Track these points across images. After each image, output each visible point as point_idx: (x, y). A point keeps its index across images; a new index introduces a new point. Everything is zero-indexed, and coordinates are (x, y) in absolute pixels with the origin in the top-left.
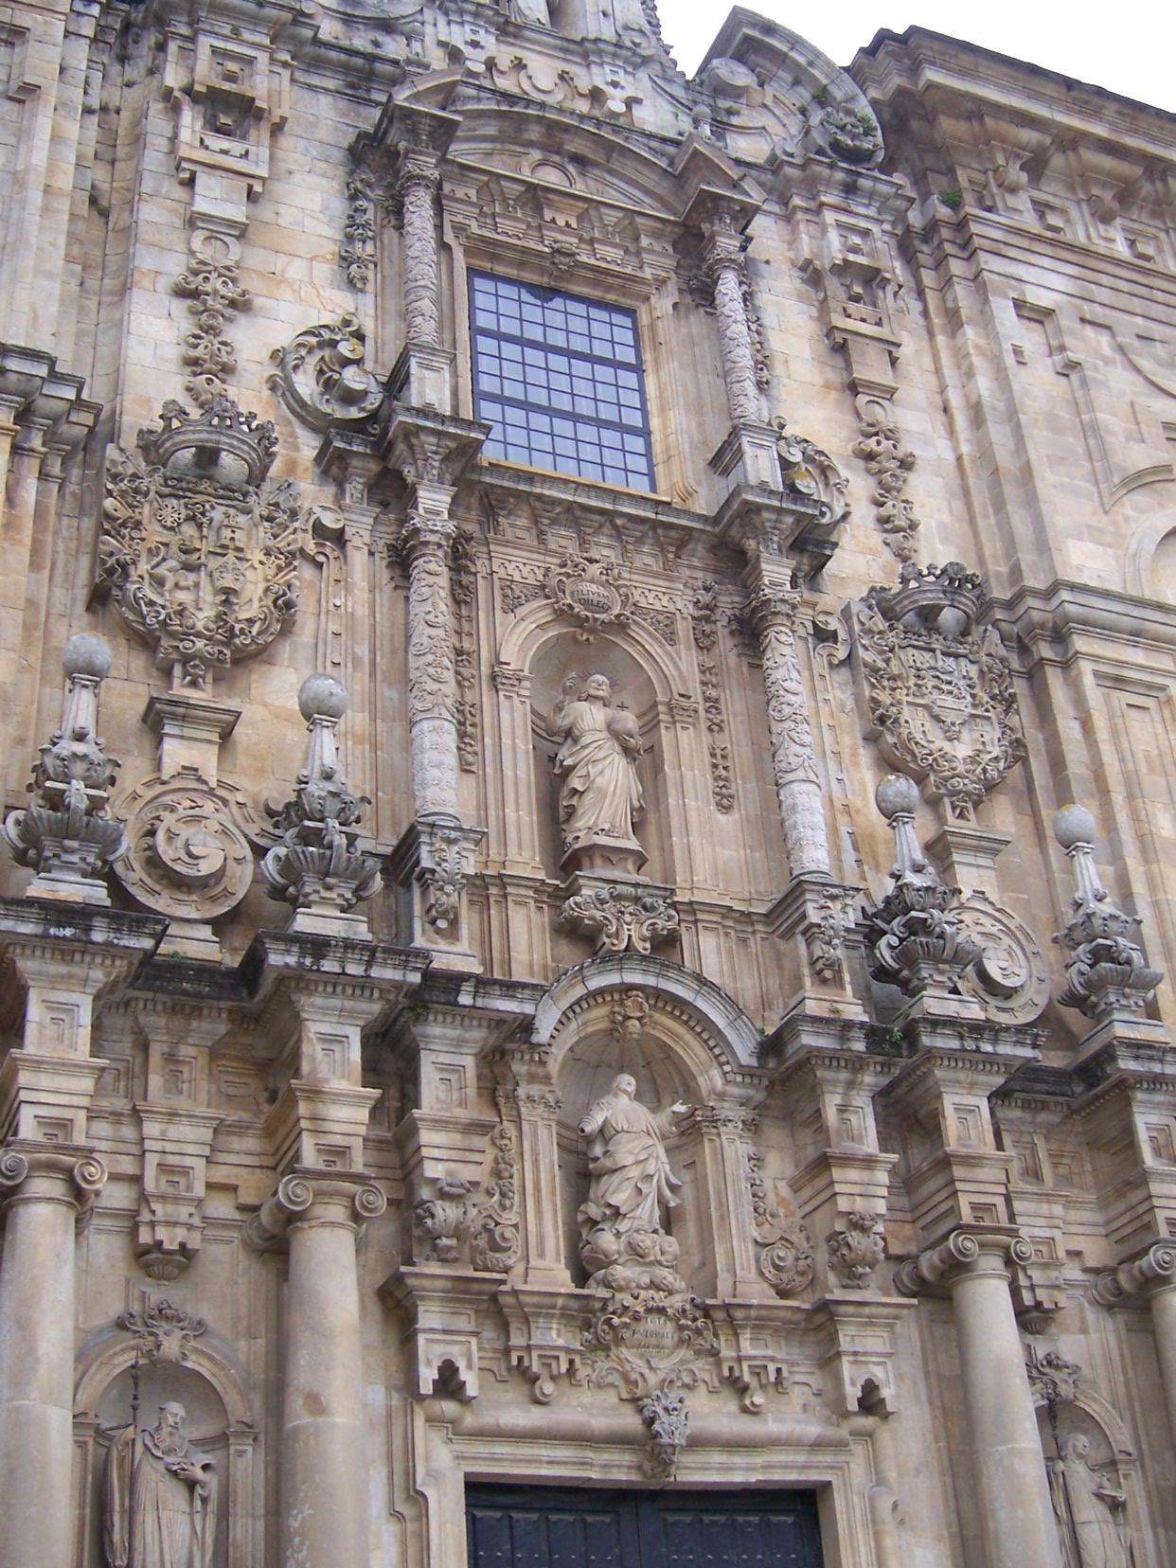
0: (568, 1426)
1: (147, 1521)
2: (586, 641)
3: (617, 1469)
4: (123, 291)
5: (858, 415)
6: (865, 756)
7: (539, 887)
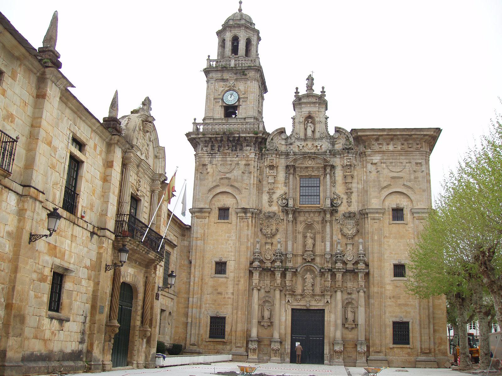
0: (301, 304)
1: (265, 313)
2: (309, 226)
3: (305, 308)
4: (262, 193)
5: (346, 187)
6: (340, 233)
7: (301, 255)
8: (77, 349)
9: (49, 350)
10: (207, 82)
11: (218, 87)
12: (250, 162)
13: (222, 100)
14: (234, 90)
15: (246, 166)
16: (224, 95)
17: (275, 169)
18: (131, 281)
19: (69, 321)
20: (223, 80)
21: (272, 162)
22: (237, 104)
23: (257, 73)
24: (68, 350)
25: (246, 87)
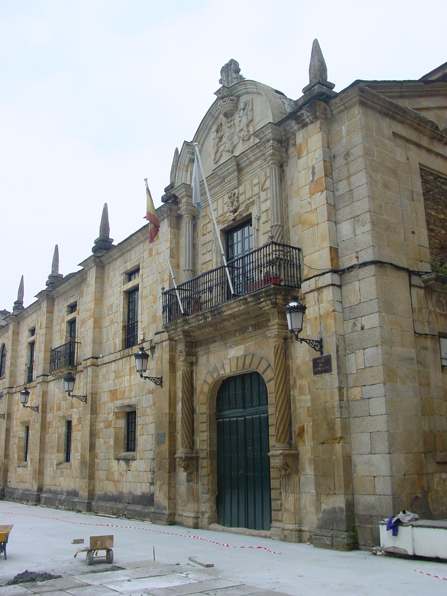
8: (148, 491)
9: (119, 492)
18: (234, 369)
19: (135, 460)
24: (138, 492)
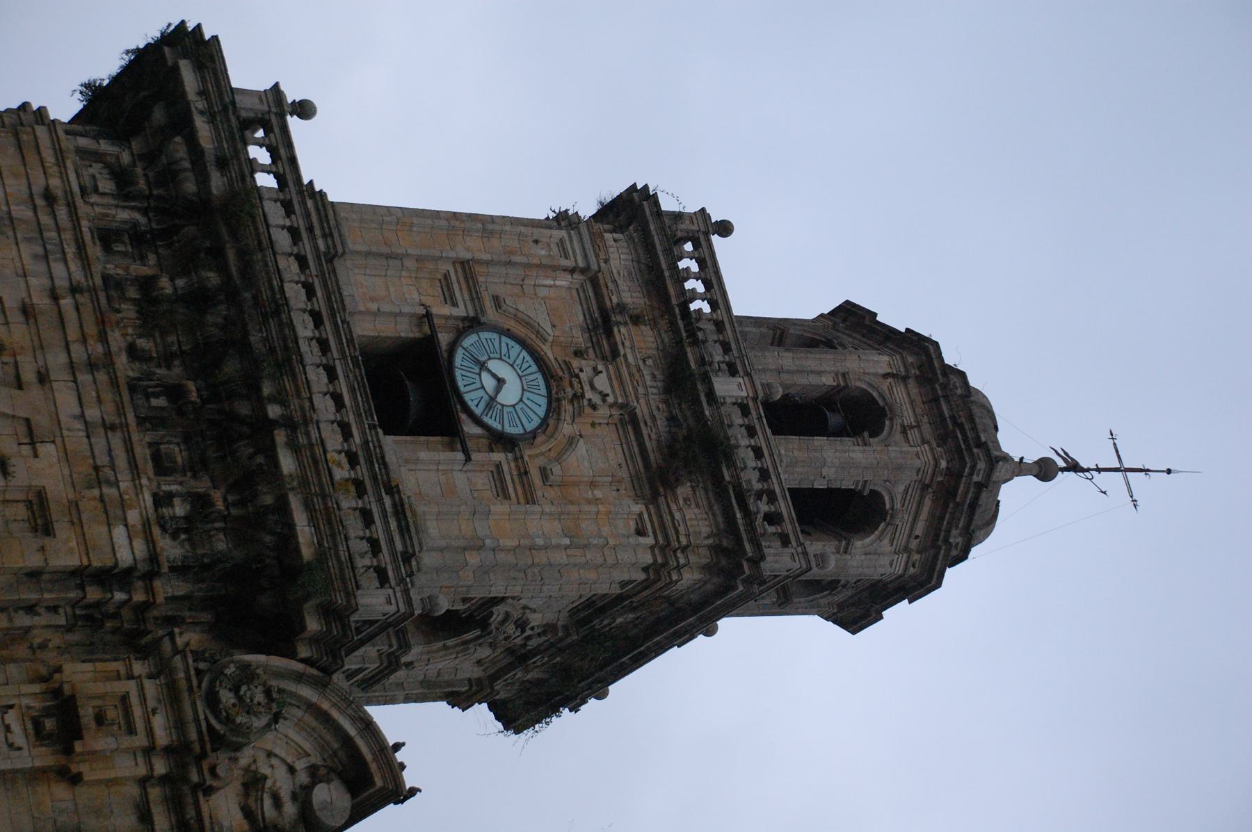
10: (564, 220)
11: (543, 292)
12: (63, 529)
13: (473, 324)
14: (554, 406)
15: (21, 512)
16: (508, 333)
17: (44, 757)
20: (602, 323)
21: (100, 719)
22: (470, 428)
23: (705, 568)
25: (598, 493)
